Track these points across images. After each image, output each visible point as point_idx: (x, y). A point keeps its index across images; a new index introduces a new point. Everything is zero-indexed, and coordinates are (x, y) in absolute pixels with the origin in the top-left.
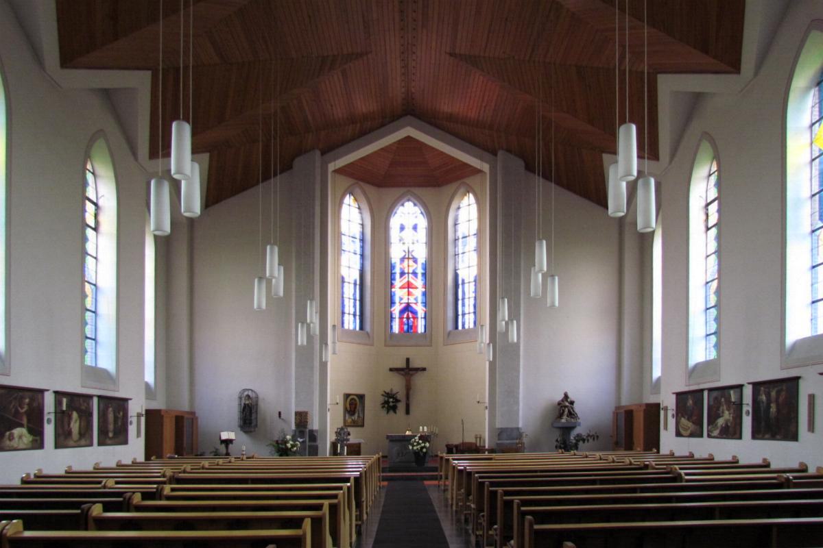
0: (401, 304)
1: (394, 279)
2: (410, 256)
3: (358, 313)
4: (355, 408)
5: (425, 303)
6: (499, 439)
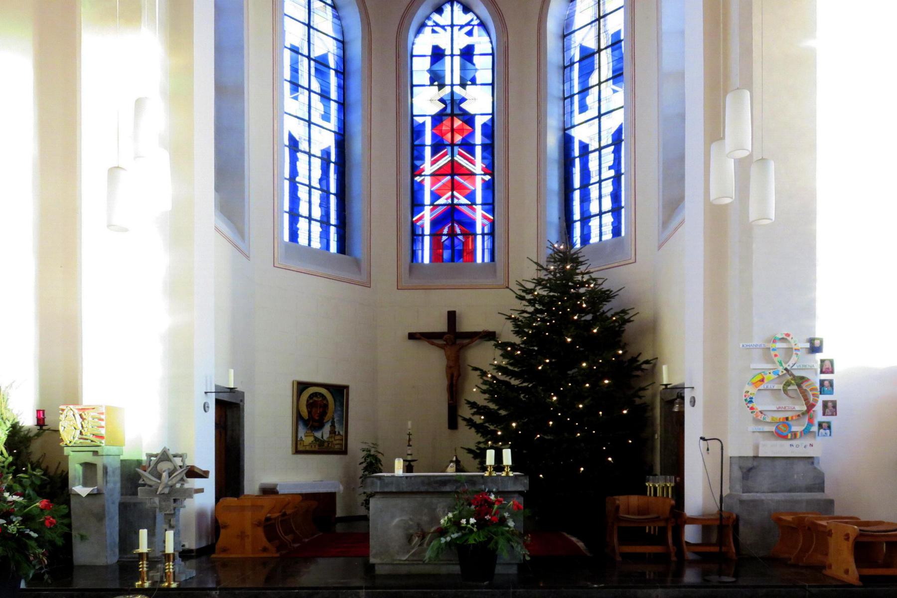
0: (434, 207)
1: (422, 158)
2: (457, 111)
3: (333, 220)
4: (324, 413)
5: (493, 204)
6: (746, 490)
